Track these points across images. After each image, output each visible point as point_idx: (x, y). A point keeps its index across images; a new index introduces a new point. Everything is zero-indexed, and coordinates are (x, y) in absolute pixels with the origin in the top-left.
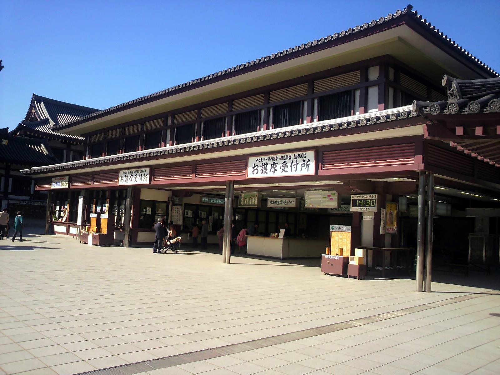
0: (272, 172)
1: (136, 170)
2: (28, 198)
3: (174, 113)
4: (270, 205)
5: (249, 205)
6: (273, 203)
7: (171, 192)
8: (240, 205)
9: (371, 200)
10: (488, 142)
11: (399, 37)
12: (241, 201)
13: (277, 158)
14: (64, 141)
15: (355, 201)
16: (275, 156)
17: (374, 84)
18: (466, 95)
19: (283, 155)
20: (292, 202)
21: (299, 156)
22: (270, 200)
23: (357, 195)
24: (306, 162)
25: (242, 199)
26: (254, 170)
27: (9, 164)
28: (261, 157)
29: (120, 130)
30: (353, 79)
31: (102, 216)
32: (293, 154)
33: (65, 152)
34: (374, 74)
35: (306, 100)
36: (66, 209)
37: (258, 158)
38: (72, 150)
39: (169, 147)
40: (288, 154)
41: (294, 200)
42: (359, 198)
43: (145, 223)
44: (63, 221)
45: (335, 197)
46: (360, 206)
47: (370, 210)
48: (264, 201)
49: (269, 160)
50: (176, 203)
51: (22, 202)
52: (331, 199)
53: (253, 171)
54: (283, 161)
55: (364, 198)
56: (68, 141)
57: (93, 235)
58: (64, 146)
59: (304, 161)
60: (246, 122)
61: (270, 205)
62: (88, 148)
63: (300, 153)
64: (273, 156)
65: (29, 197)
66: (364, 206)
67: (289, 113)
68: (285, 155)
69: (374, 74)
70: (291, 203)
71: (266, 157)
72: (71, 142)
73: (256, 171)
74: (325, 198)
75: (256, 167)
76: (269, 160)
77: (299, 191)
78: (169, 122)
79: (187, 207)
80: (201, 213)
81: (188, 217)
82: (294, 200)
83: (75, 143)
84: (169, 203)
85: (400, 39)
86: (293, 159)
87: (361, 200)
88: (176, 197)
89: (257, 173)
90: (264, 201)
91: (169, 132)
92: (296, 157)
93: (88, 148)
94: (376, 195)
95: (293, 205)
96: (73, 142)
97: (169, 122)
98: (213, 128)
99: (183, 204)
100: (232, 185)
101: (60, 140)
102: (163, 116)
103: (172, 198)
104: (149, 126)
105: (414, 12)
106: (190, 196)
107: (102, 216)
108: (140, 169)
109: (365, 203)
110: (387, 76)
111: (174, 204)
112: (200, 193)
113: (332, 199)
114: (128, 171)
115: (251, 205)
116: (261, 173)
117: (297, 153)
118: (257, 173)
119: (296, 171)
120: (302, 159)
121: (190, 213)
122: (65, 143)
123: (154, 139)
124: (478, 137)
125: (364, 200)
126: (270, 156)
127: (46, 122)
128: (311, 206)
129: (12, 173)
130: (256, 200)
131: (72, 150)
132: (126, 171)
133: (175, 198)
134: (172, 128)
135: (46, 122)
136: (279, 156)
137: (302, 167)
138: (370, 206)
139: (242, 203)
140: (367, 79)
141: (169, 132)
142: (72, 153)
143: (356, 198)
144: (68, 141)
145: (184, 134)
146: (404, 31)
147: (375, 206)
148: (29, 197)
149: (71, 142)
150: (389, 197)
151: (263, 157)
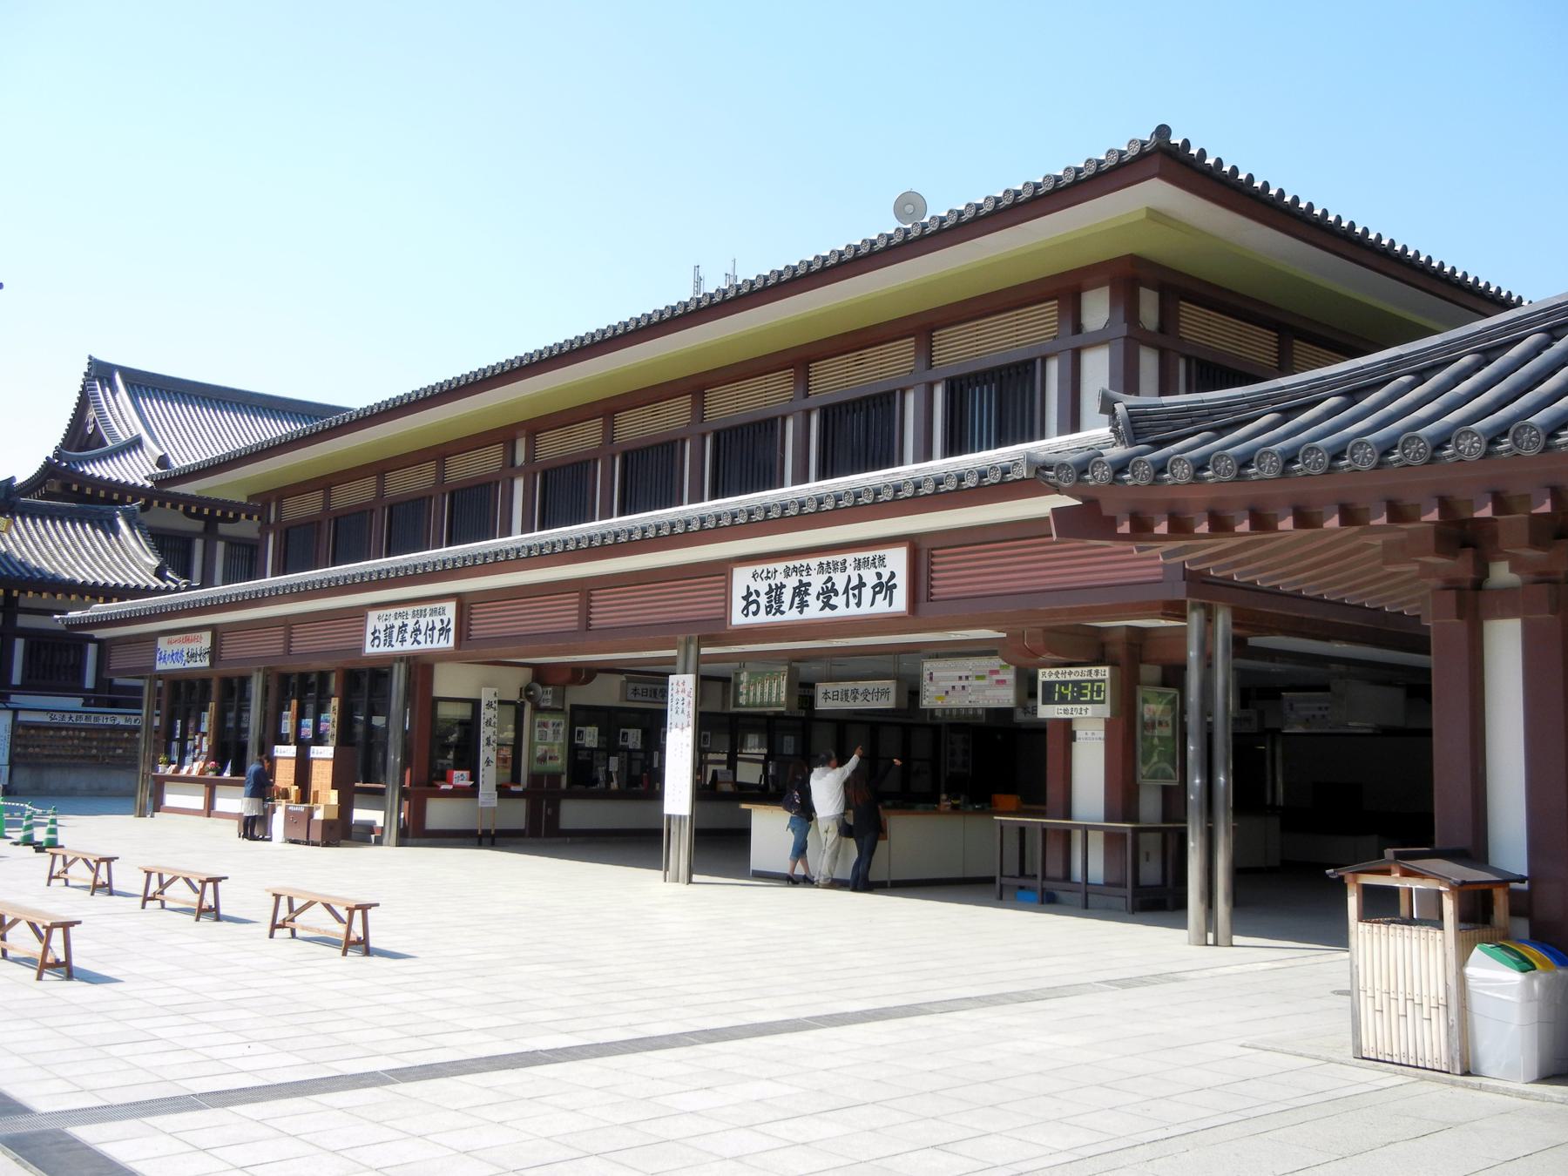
0: (795, 610)
1: (417, 608)
2: (76, 703)
3: (534, 428)
4: (822, 704)
5: (762, 705)
6: (828, 699)
7: (528, 672)
8: (737, 704)
9: (1093, 682)
10: (1210, 546)
11: (1149, 210)
12: (737, 694)
13: (808, 568)
14: (194, 510)
15: (1049, 686)
16: (804, 562)
17: (1097, 341)
18: (1145, 434)
19: (824, 560)
20: (886, 692)
21: (866, 561)
22: (821, 688)
23: (1054, 670)
24: (884, 580)
25: (743, 689)
26: (749, 604)
27: (15, 593)
28: (765, 567)
29: (371, 481)
30: (1040, 323)
31: (316, 752)
32: (850, 557)
33: (199, 545)
34: (1097, 310)
35: (911, 388)
36: (204, 734)
37: (759, 568)
38: (222, 538)
39: (518, 538)
40: (839, 558)
41: (890, 685)
42: (1061, 678)
43: (406, 760)
44: (194, 773)
45: (1009, 676)
46: (1063, 700)
47: (1089, 714)
48: (804, 691)
49: (787, 575)
50: (543, 704)
51: (58, 716)
52: (998, 682)
53: (746, 608)
54: (826, 576)
55: (1073, 678)
56: (206, 511)
57: (287, 813)
58: (198, 525)
59: (879, 575)
60: (745, 457)
61: (822, 704)
62: (271, 538)
63: (870, 554)
64: (797, 563)
65: (81, 700)
66: (1076, 701)
67: (859, 434)
68: (830, 558)
69: (1097, 310)
70: (880, 696)
71: (780, 566)
72: (219, 513)
73: (753, 608)
74: (983, 677)
75: (754, 597)
76: (787, 575)
77: (906, 664)
78: (520, 458)
79: (581, 715)
80: (625, 734)
81: (583, 748)
82: (890, 685)
83: (231, 515)
84: (523, 704)
85: (1154, 215)
86: (850, 570)
87: (1065, 684)
88: (544, 685)
89: (755, 613)
90: (804, 691)
91: (519, 485)
92: (859, 564)
93: (271, 538)
94: (1107, 669)
95: (888, 703)
96: (224, 514)
97: (520, 458)
98: (649, 476)
99: (568, 708)
100: (693, 648)
101: (181, 507)
102: (504, 436)
103: (528, 688)
104: (463, 469)
105: (1179, 142)
106: (588, 680)
107: (316, 752)
108: (428, 607)
109: (1077, 692)
110: (1132, 315)
111: (537, 709)
112: (621, 672)
113: (1002, 682)
114: (392, 611)
115: (770, 704)
116: (768, 613)
117: (861, 555)
118: (755, 613)
119: (859, 604)
120: (873, 571)
121: (590, 737)
122: (198, 515)
123: (473, 511)
124: (1161, 538)
125: (1076, 683)
126: (791, 564)
127: (136, 444)
128: (956, 702)
129: (24, 621)
130: (784, 689)
131: (222, 538)
132: (388, 612)
133: (540, 689)
134: (528, 473)
135: (136, 444)
136: (813, 562)
137: (875, 594)
138: (1092, 702)
139: (742, 700)
140: (1078, 328)
141: (519, 485)
142: (220, 546)
143: (1053, 678)
144: (206, 511)
145: (562, 495)
146: (1156, 193)
147: (1103, 702)
148: (81, 700)
149: (219, 513)
150: (1150, 672)
151: (771, 567)
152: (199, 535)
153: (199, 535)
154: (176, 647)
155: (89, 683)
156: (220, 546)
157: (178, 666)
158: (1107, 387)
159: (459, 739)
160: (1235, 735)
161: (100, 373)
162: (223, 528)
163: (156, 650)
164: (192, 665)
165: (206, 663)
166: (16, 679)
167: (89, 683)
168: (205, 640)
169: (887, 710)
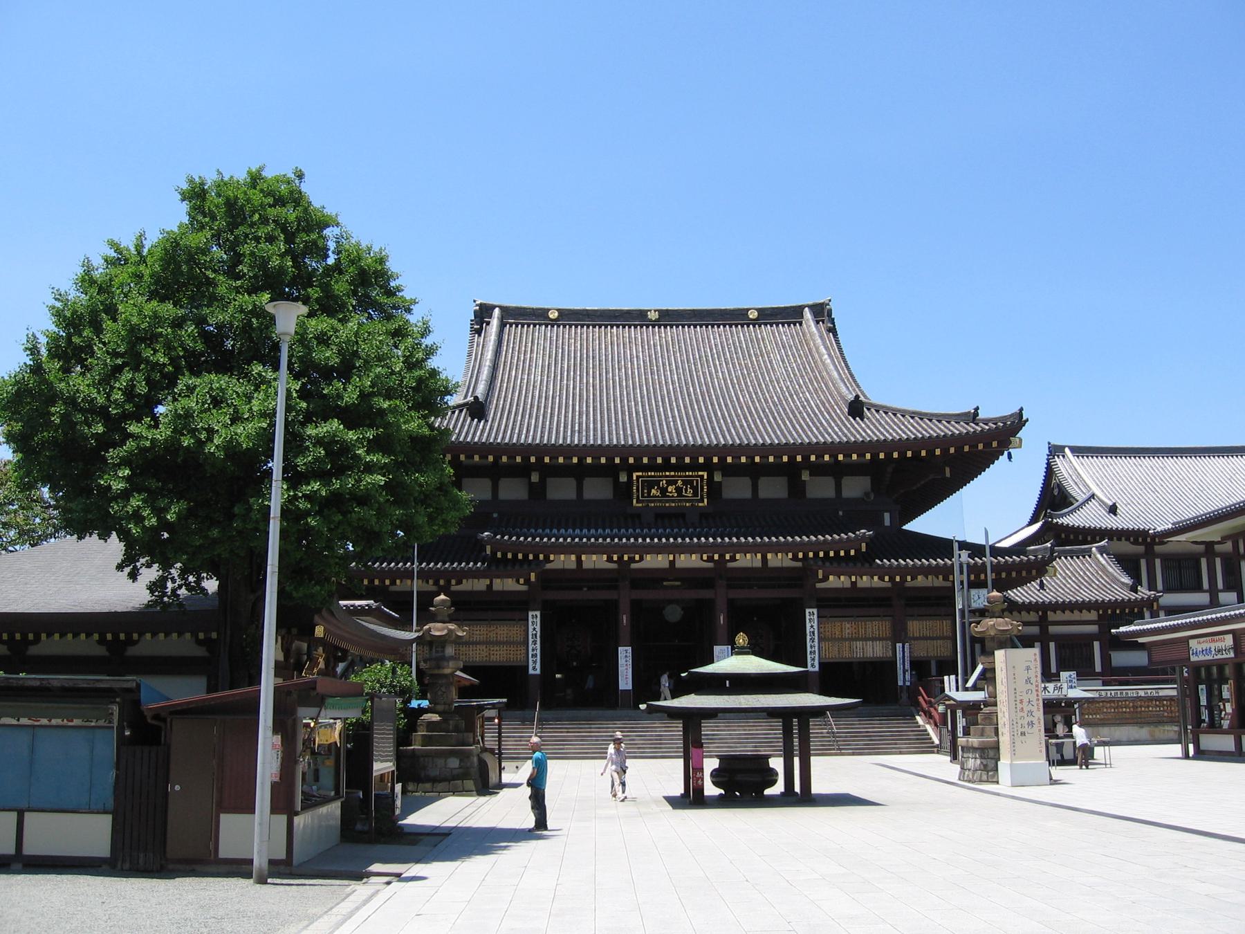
36: (1228, 701)
38: (1159, 556)
58: (1141, 549)
152: (1142, 556)
153: (1142, 556)
154: (1205, 646)
155: (1098, 668)
157: (1210, 657)
158: (251, 881)
159: (336, 666)
160: (851, 663)
161: (1055, 451)
162: (1157, 548)
163: (1189, 648)
164: (1219, 656)
165: (1232, 655)
166: (1096, 645)
167: (1098, 668)
168: (1229, 640)
169: (565, 501)
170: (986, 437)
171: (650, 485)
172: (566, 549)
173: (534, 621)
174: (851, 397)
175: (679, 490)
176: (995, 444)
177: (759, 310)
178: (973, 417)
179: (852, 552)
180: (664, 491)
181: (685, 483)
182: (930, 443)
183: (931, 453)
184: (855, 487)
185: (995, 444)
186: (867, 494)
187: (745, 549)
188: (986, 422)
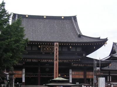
33: (108, 77)
58: (108, 74)
129: (111, 74)
156: (111, 77)
170: (101, 42)
171: (44, 48)
172: (30, 59)
173: (24, 71)
174: (79, 34)
175: (49, 49)
176: (102, 43)
177: (64, 17)
178: (99, 38)
179: (78, 60)
180: (46, 49)
181: (50, 48)
182: (92, 43)
183: (92, 44)
184: (79, 50)
185: (102, 43)
186: (81, 51)
187: (28, 59)
188: (101, 39)
